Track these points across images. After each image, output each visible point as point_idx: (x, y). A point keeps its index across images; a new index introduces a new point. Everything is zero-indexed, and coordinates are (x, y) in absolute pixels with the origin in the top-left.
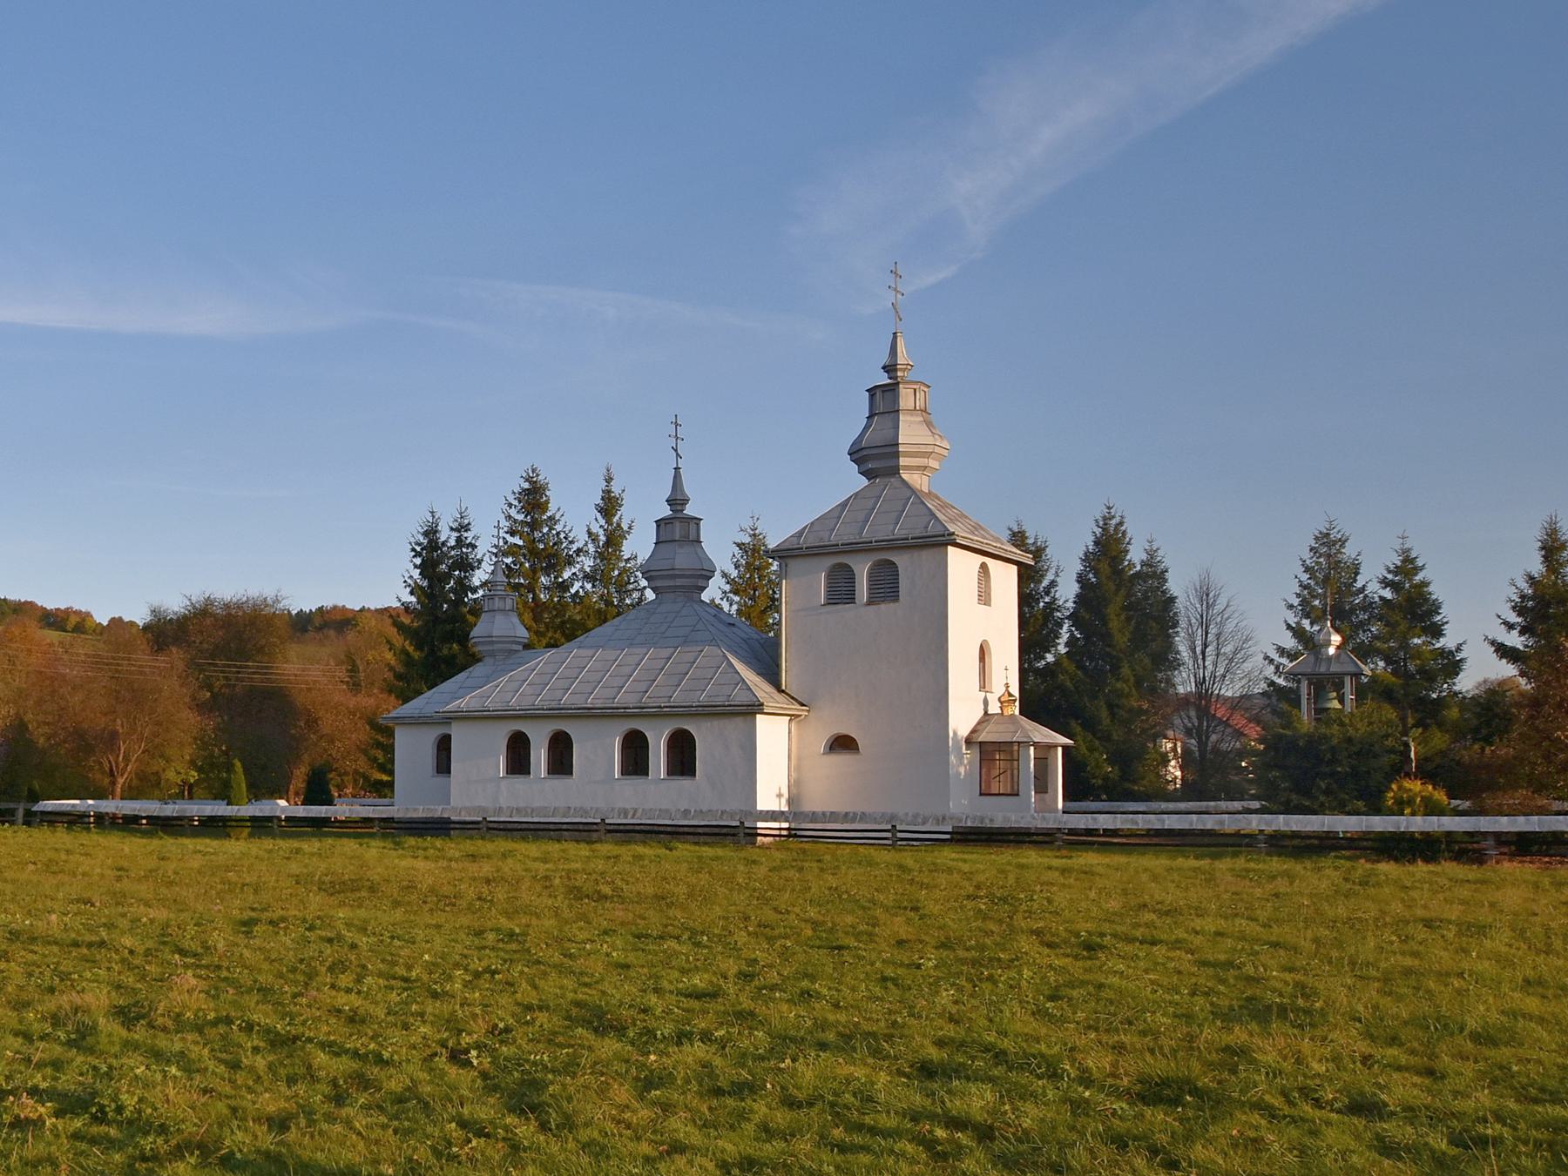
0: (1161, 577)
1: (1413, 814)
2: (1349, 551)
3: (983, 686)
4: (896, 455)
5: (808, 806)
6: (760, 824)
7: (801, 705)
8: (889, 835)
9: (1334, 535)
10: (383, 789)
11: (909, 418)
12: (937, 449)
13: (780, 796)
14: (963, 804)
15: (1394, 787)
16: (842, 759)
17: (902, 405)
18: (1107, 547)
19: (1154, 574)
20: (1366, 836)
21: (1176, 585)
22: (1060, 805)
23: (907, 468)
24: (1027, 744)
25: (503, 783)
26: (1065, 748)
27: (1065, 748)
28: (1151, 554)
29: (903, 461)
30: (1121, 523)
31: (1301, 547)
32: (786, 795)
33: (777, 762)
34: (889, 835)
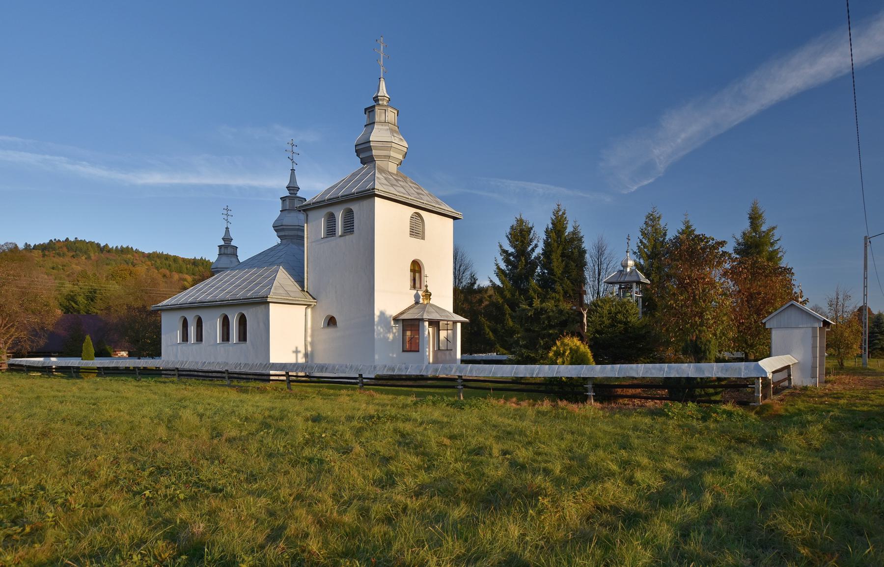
0: (580, 240)
1: (563, 363)
2: (662, 223)
3: (414, 287)
4: (370, 149)
5: (320, 360)
6: (272, 372)
7: (310, 298)
8: (284, 378)
9: (656, 215)
10: (157, 353)
11: (380, 127)
12: (394, 145)
13: (297, 352)
14: (387, 357)
15: (558, 343)
16: (331, 330)
17: (377, 119)
18: (558, 226)
19: (576, 239)
20: (517, 381)
21: (587, 245)
22: (459, 356)
23: (379, 156)
24: (422, 320)
25: (179, 347)
26: (463, 323)
27: (463, 323)
28: (575, 228)
29: (374, 152)
30: (564, 213)
31: (641, 222)
32: (303, 351)
33: (289, 334)
34: (284, 378)
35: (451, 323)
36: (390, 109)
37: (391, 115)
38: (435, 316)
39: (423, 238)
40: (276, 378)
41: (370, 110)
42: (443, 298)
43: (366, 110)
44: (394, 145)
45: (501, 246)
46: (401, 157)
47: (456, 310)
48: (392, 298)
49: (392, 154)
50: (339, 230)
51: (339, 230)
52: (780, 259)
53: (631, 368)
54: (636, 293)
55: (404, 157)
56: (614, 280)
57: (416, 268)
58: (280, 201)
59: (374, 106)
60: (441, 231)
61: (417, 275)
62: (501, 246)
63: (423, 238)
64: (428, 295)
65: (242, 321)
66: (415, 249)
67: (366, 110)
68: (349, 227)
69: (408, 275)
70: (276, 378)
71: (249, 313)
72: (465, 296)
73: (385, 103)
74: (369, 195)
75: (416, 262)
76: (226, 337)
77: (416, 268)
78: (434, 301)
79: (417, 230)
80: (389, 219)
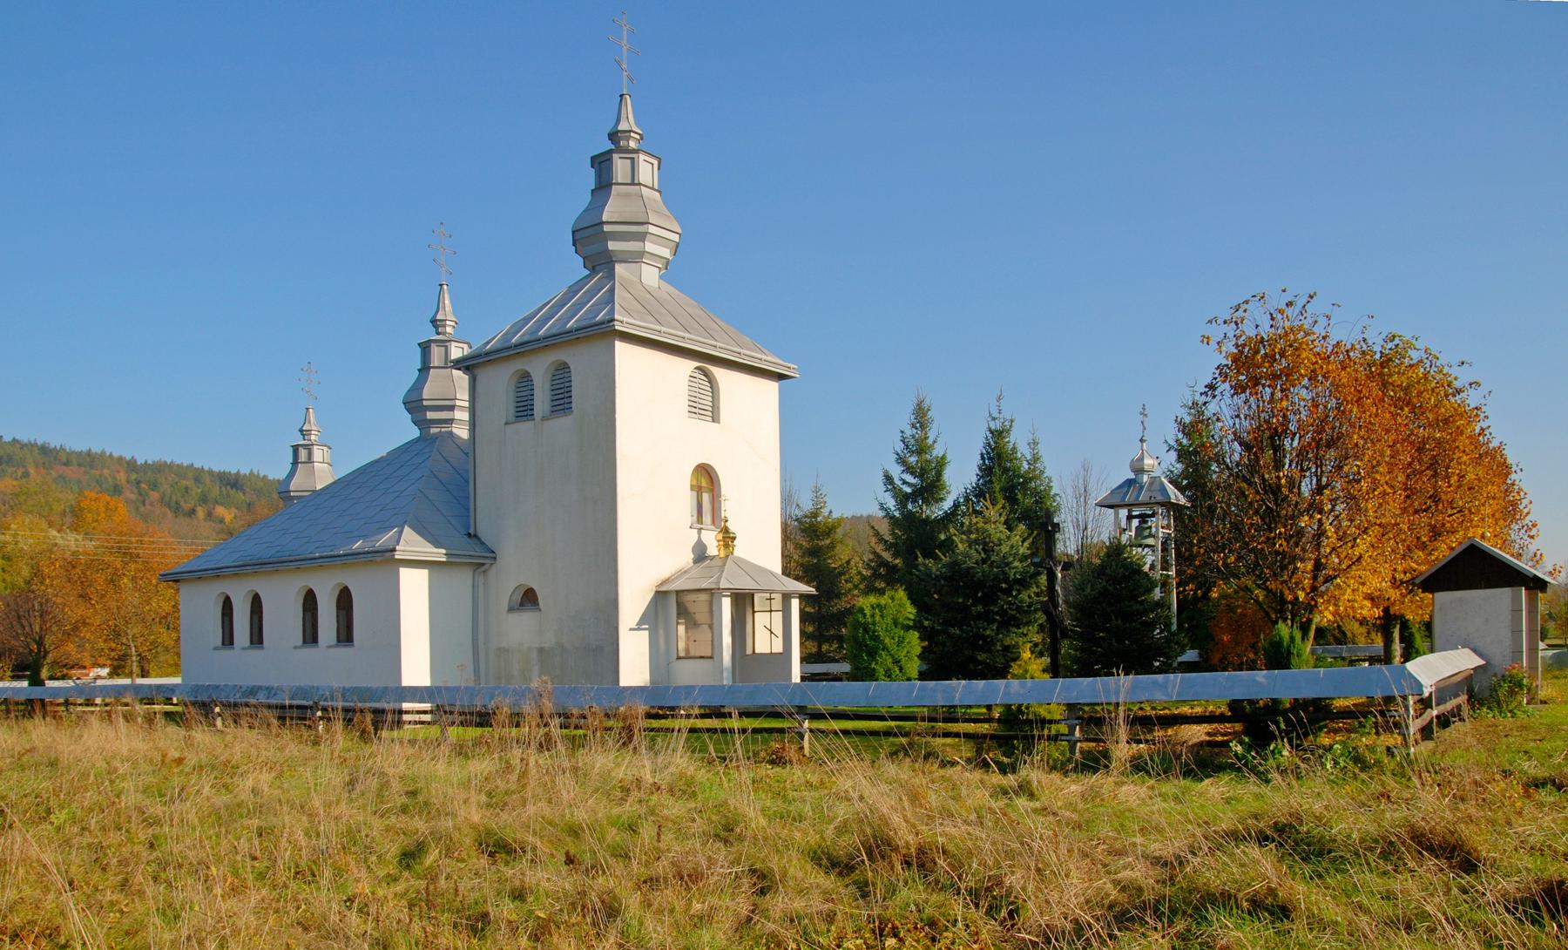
12: (652, 229)
35: (778, 598)
36: (642, 157)
37: (647, 170)
38: (744, 584)
39: (715, 418)
40: (417, 717)
41: (602, 163)
42: (761, 546)
43: (593, 158)
44: (652, 229)
45: (921, 417)
46: (666, 253)
47: (786, 572)
48: (651, 546)
49: (649, 247)
50: (542, 402)
51: (542, 402)
52: (1006, 478)
53: (1155, 682)
54: (1161, 526)
55: (676, 248)
56: (1116, 501)
57: (706, 479)
58: (419, 350)
59: (610, 152)
60: (752, 404)
61: (706, 497)
62: (921, 417)
63: (715, 418)
64: (728, 538)
65: (345, 601)
66: (704, 443)
67: (593, 158)
68: (562, 401)
69: (686, 499)
70: (417, 717)
71: (360, 584)
72: (809, 544)
73: (632, 144)
74: (603, 333)
75: (703, 475)
76: (311, 636)
77: (706, 479)
78: (740, 550)
79: (708, 408)
80: (646, 388)
